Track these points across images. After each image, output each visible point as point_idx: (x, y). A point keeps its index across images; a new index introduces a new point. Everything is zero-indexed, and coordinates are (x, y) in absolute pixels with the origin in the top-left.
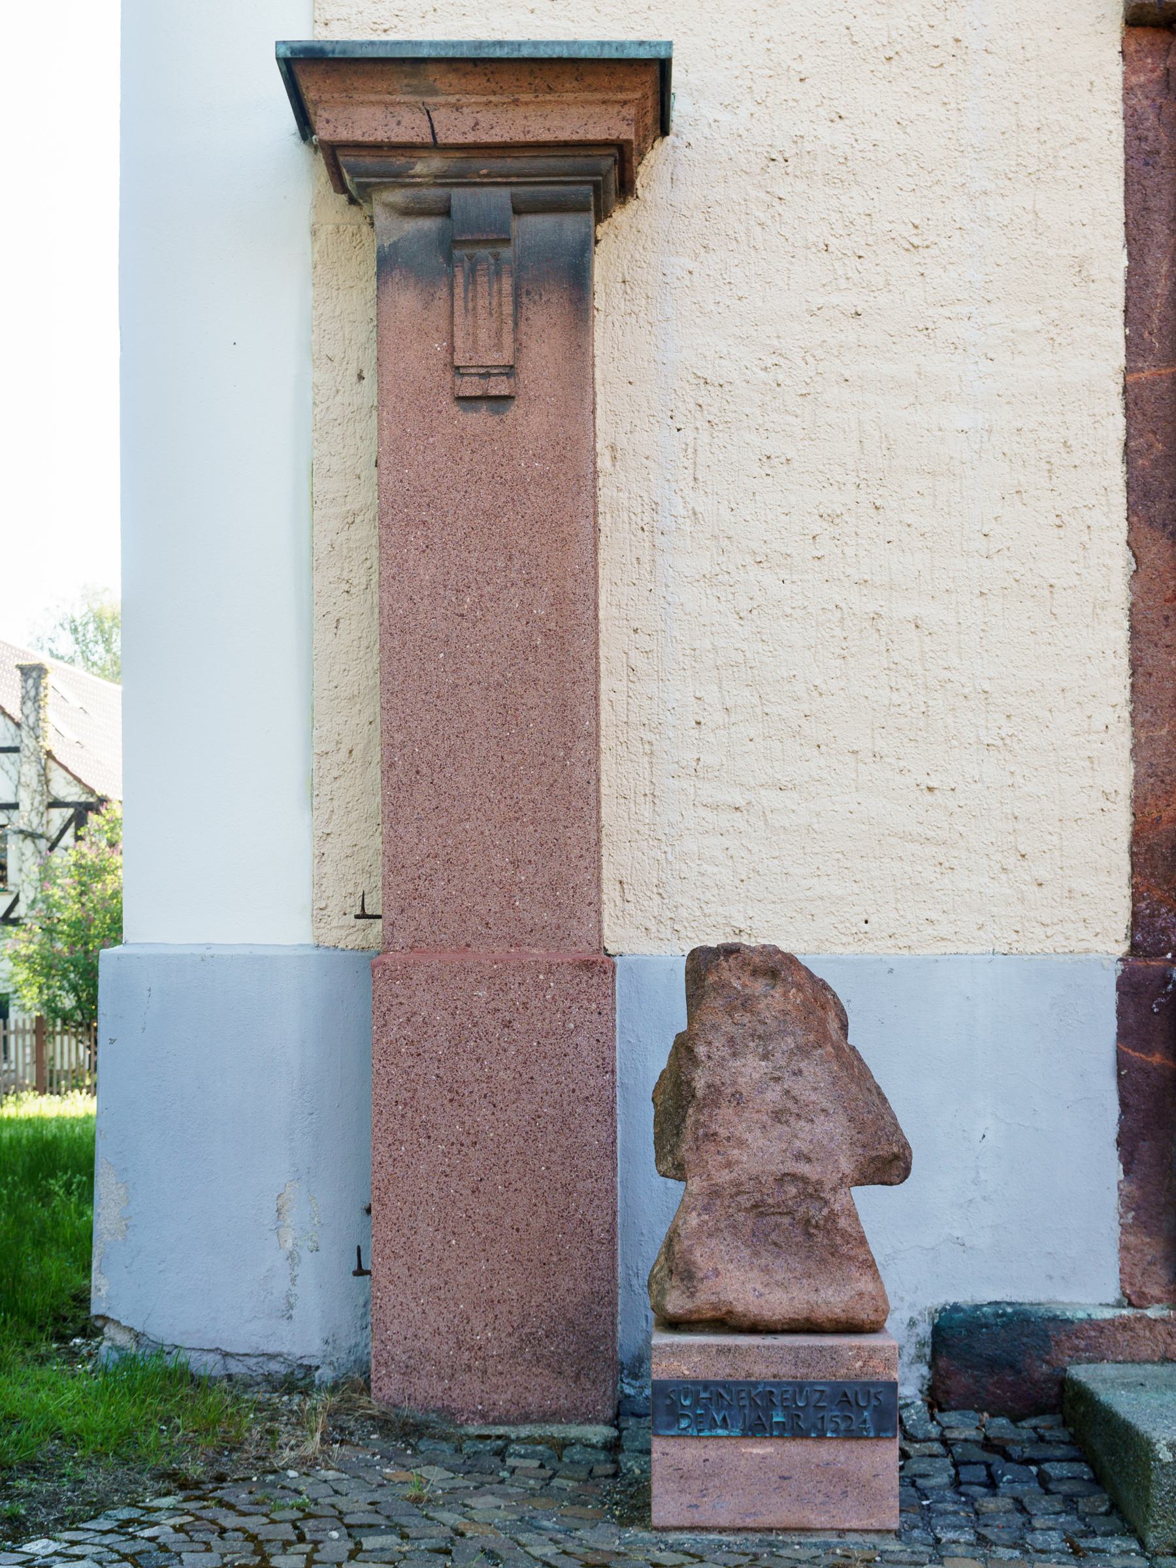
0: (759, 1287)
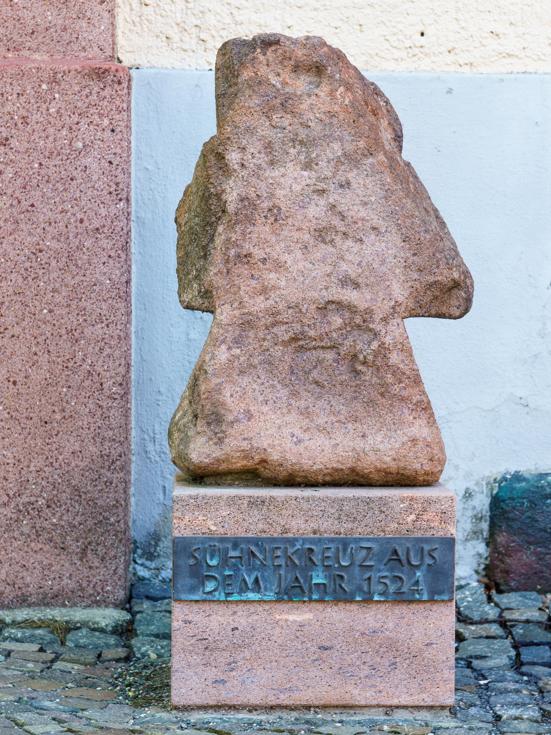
0: (298, 432)
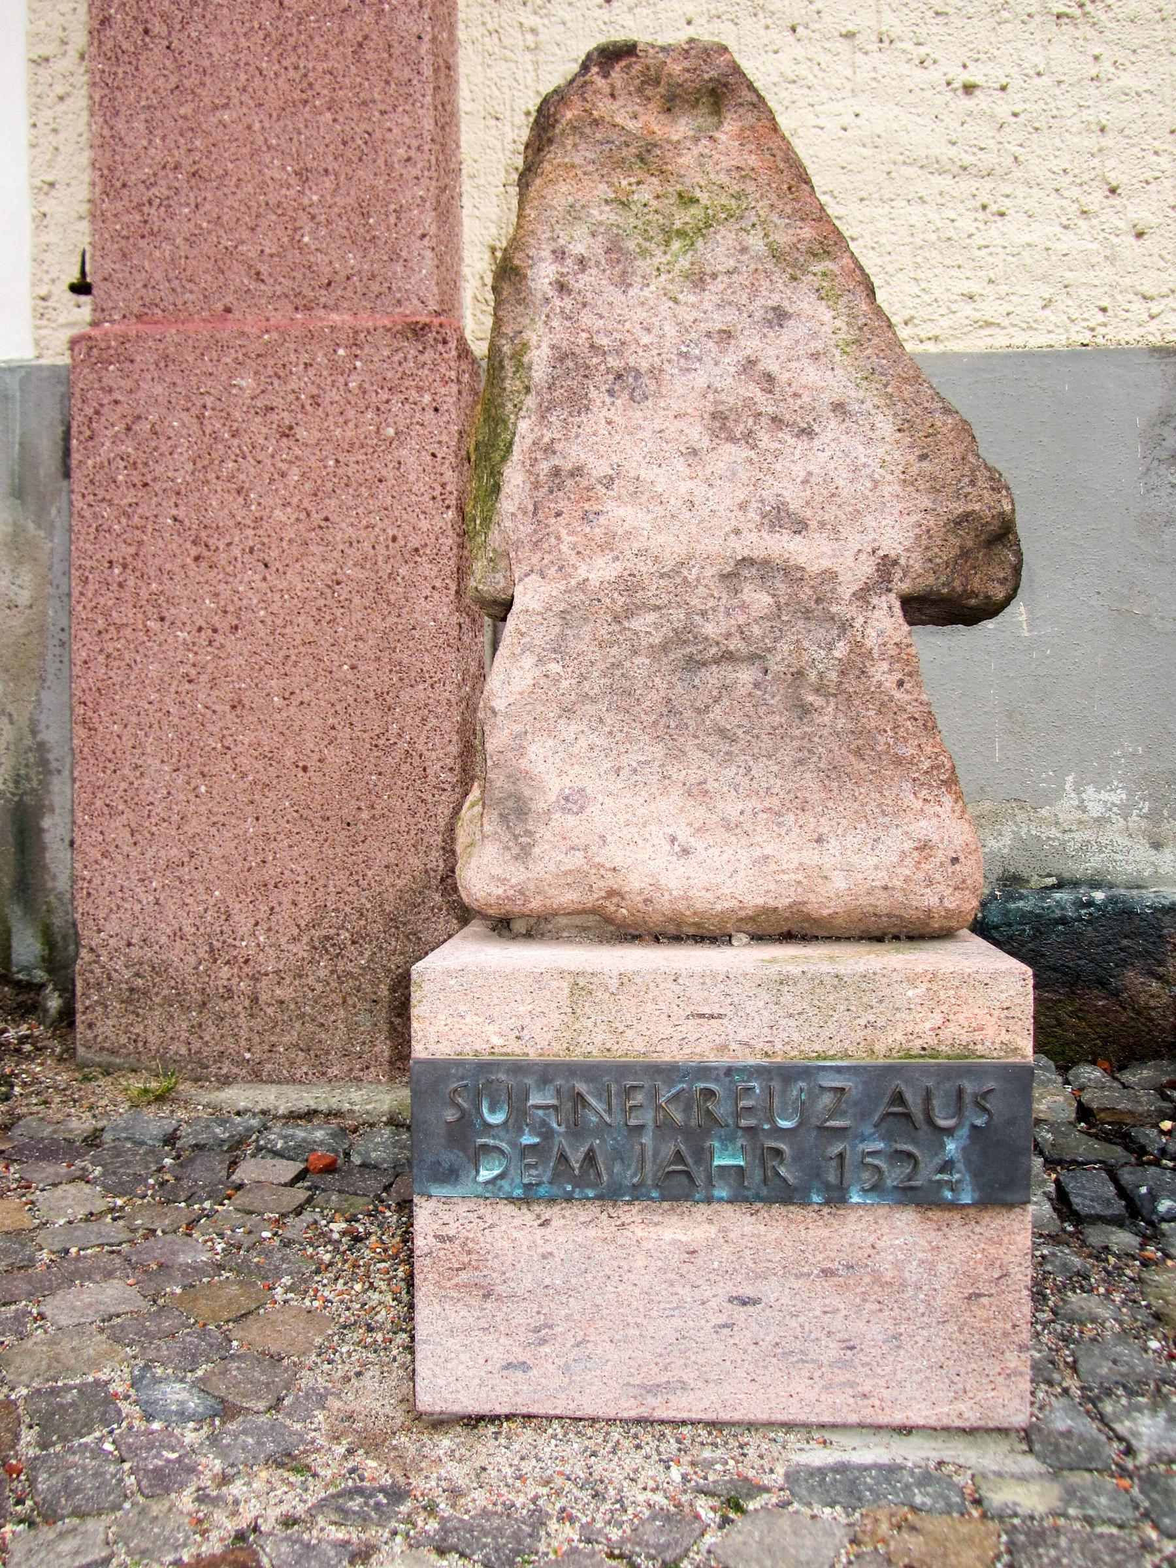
0: (684, 835)
